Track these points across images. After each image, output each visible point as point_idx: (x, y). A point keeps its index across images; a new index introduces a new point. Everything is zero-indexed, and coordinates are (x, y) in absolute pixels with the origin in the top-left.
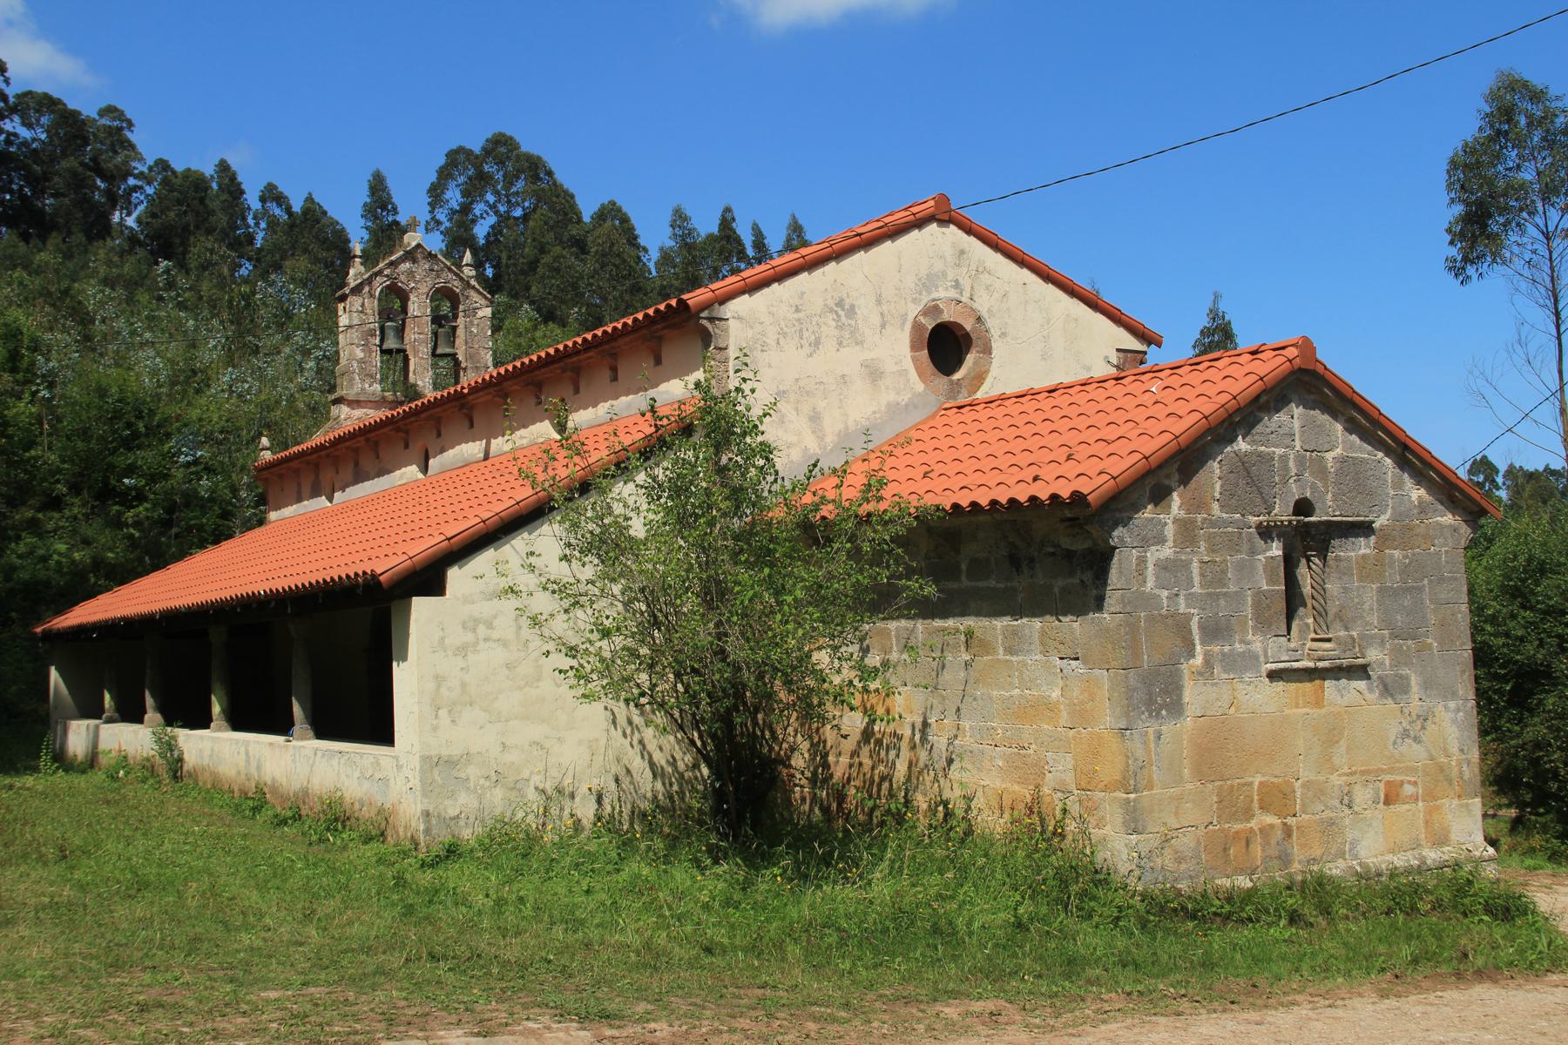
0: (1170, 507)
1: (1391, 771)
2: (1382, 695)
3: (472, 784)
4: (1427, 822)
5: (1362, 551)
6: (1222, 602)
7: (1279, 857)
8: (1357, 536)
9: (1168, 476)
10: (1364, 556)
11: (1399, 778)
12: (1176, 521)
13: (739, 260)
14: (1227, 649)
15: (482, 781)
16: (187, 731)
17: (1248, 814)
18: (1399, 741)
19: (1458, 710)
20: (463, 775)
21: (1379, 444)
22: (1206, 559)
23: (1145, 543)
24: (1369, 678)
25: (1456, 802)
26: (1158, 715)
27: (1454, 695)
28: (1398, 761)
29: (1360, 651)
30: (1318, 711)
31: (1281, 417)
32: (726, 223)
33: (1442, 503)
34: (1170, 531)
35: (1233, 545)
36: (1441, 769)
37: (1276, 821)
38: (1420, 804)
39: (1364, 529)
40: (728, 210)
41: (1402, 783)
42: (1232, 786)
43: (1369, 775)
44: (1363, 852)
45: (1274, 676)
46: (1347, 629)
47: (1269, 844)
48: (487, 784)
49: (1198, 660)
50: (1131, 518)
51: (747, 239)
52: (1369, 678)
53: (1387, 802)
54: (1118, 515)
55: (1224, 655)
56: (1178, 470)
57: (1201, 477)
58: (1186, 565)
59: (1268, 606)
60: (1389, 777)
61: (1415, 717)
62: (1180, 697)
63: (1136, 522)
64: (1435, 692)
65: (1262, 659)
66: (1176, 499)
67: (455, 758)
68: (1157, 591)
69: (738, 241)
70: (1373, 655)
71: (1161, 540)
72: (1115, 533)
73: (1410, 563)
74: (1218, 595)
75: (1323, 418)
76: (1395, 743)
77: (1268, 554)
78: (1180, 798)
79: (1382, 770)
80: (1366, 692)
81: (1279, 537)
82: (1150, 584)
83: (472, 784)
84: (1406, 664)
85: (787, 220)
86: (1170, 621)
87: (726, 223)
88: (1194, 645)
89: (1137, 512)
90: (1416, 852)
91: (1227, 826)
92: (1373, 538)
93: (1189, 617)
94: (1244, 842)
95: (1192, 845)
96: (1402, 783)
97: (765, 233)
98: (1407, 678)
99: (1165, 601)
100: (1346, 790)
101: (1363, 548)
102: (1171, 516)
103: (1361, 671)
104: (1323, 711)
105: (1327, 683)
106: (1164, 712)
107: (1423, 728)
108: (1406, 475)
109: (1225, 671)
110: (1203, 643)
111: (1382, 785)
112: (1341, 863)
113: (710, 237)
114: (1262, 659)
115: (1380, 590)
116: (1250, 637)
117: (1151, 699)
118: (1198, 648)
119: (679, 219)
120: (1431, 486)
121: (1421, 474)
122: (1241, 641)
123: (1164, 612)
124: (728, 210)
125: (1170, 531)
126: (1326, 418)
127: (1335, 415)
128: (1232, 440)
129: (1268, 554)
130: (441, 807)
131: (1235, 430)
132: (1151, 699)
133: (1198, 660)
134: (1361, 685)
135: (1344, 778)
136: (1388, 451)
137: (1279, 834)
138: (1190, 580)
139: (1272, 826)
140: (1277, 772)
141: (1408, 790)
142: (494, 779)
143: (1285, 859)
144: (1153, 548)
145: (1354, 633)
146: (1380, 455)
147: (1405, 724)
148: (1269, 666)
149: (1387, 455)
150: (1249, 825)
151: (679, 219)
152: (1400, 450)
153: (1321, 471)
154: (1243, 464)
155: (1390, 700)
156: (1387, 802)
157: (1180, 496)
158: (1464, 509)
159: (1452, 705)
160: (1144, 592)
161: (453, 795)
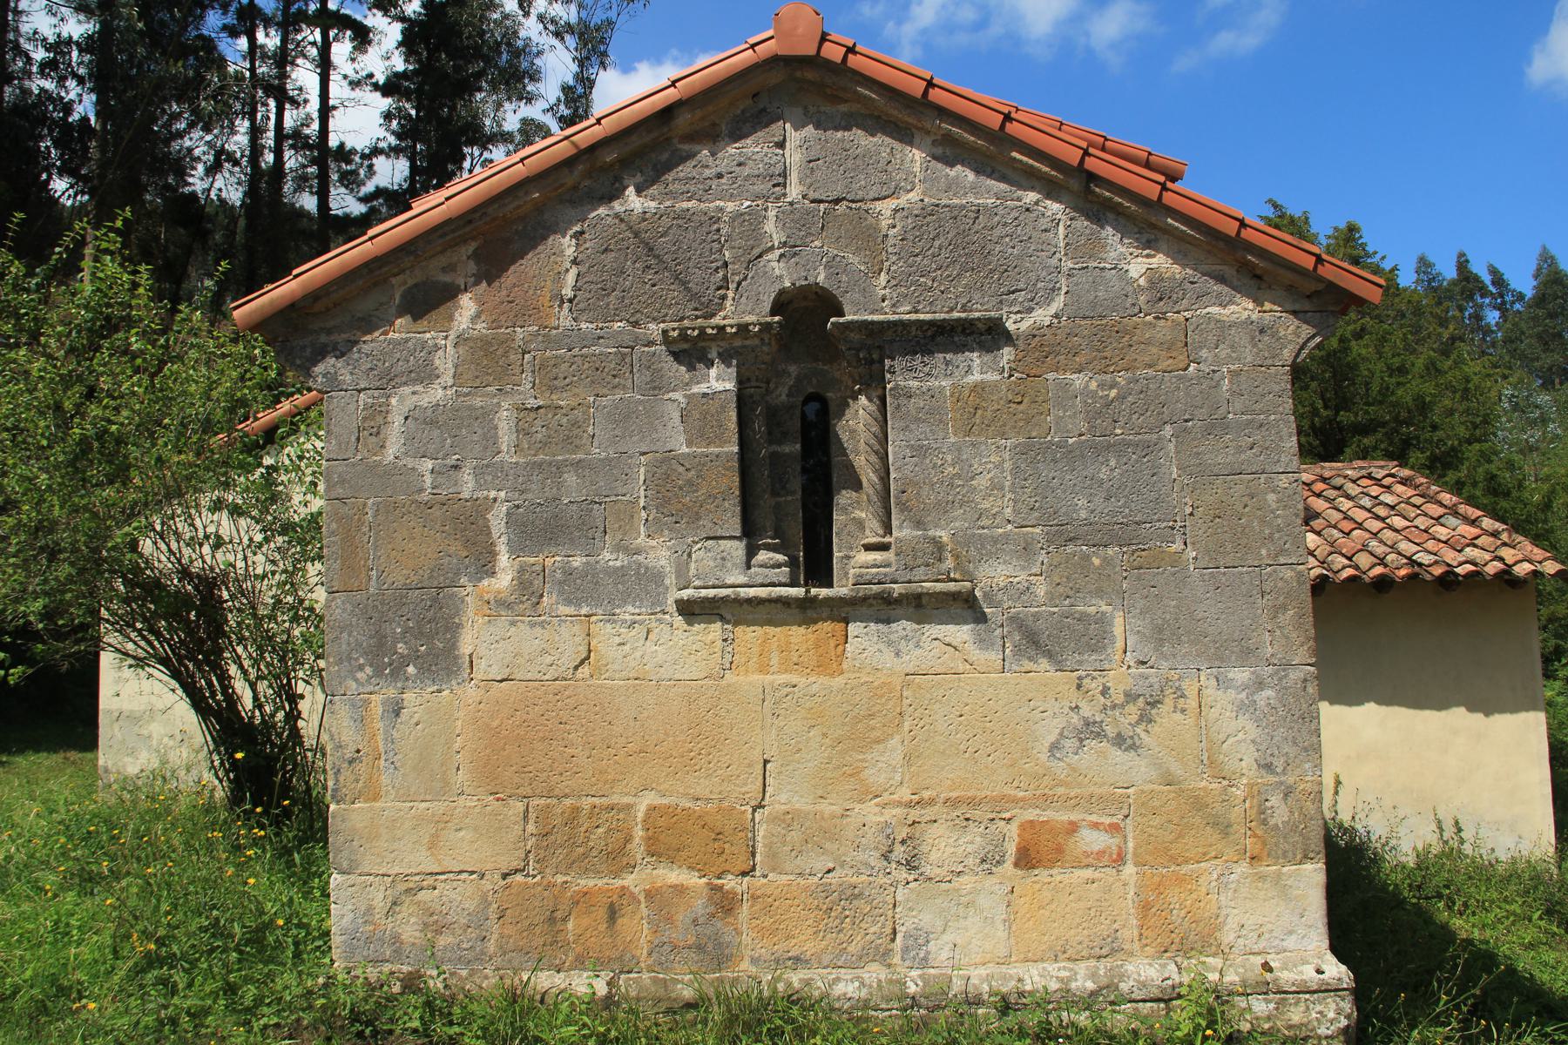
0: (451, 318)
1: (1046, 800)
2: (1018, 652)
3: (154, 742)
4: (1145, 908)
5: (976, 377)
6: (570, 478)
7: (700, 948)
8: (961, 348)
9: (450, 268)
10: (978, 388)
11: (1064, 817)
12: (461, 340)
13: (1482, 296)
14: (577, 562)
15: (166, 740)
16: (1339, 710)
17: (617, 859)
18: (1070, 744)
19: (1260, 685)
20: (145, 732)
21: (1028, 179)
22: (532, 403)
23: (387, 382)
24: (981, 618)
25: (1242, 868)
26: (397, 672)
27: (1247, 654)
28: (1061, 784)
29: (958, 567)
30: (823, 680)
31: (754, 147)
32: (1462, 265)
33: (1221, 279)
34: (445, 362)
35: (604, 375)
36: (1198, 803)
37: (694, 880)
38: (1129, 870)
39: (989, 335)
40: (1462, 255)
41: (1073, 828)
42: (576, 810)
43: (964, 809)
44: (940, 951)
45: (691, 611)
46: (919, 524)
47: (669, 919)
48: (171, 743)
49: (504, 579)
50: (356, 343)
51: (1487, 279)
52: (981, 618)
53: (1026, 860)
54: (323, 338)
55: (569, 573)
56: (476, 256)
57: (529, 265)
58: (485, 417)
59: (690, 483)
60: (1031, 814)
61: (1120, 699)
62: (452, 646)
63: (366, 348)
64: (1185, 648)
65: (670, 580)
66: (467, 305)
67: (137, 715)
68: (410, 462)
69: (1477, 279)
70: (994, 575)
71: (426, 375)
72: (319, 369)
73: (1121, 397)
74: (560, 467)
75: (861, 139)
76: (1054, 747)
77: (696, 389)
78: (442, 821)
79: (1015, 801)
80: (970, 647)
81: (725, 358)
82: (393, 448)
83: (154, 742)
84: (1099, 593)
85: (1538, 251)
86: (437, 512)
87: (1462, 265)
88: (493, 554)
89: (370, 332)
90: (1102, 967)
91: (560, 879)
92: (1007, 353)
93: (481, 508)
94: (602, 913)
95: (470, 905)
96: (1073, 828)
97: (1502, 270)
98: (1102, 620)
99: (428, 480)
100: (903, 833)
101: (976, 369)
102: (452, 335)
103: (965, 606)
104: (839, 681)
105: (854, 628)
106: (411, 669)
107: (1145, 718)
108: (1109, 230)
109: (568, 602)
110: (516, 550)
111: (1013, 830)
112: (874, 973)
113: (1453, 283)
114: (670, 580)
115: (1022, 452)
116: (641, 540)
117: (381, 644)
118: (504, 559)
119: (1424, 264)
120: (1180, 248)
121: (1153, 226)
122: (618, 548)
123: (425, 497)
124: (1462, 255)
125: (445, 362)
126: (880, 144)
127: (905, 135)
128: (615, 194)
129: (696, 389)
130: (120, 764)
131: (618, 179)
132: (381, 644)
133: (504, 579)
134: (961, 633)
135: (898, 811)
136: (1051, 190)
137: (700, 905)
138: (491, 439)
139: (680, 890)
140: (699, 791)
141: (1091, 840)
142: (179, 738)
143: (717, 954)
144: (407, 390)
145: (944, 535)
146: (1031, 197)
147: (1086, 711)
148: (686, 594)
149: (1049, 195)
150: (618, 883)
151: (1424, 264)
152: (1075, 184)
153: (868, 238)
154: (636, 235)
155: (1044, 663)
156: (1026, 860)
157: (481, 302)
158: (1290, 288)
159: (1241, 675)
160: (379, 464)
161: (132, 752)
